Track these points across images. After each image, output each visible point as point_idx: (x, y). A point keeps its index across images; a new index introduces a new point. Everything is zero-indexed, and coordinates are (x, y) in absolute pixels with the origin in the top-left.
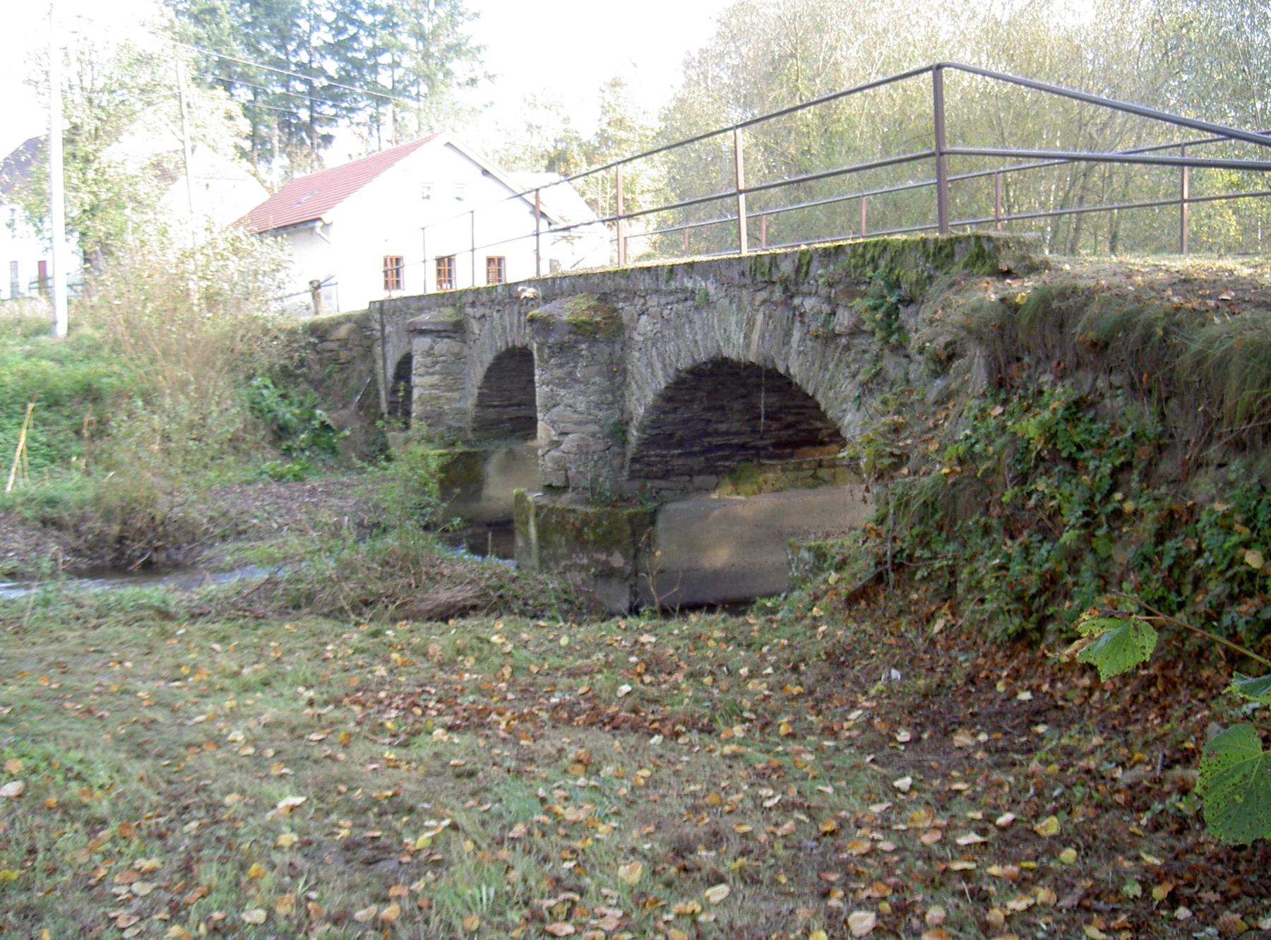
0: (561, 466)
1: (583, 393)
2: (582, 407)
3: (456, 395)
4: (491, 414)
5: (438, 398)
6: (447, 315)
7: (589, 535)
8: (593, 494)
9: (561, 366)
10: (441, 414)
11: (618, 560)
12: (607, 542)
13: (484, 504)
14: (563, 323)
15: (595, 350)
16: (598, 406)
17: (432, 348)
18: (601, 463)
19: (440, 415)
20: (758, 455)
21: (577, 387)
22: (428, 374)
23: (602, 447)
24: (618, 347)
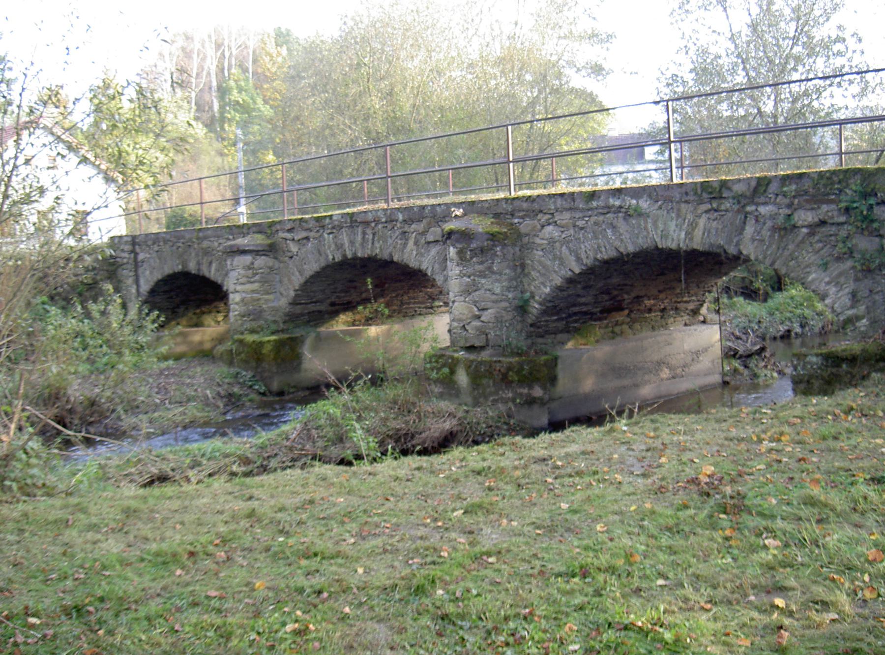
0: (482, 332)
1: (497, 281)
2: (498, 290)
3: (271, 297)
4: (298, 309)
5: (259, 300)
8: (504, 349)
9: (482, 263)
10: (261, 311)
11: (538, 392)
12: (529, 380)
13: (302, 374)
14: (481, 234)
15: (505, 251)
16: (508, 289)
17: (253, 263)
18: (511, 328)
19: (261, 312)
20: (591, 319)
23: (510, 317)
24: (517, 249)
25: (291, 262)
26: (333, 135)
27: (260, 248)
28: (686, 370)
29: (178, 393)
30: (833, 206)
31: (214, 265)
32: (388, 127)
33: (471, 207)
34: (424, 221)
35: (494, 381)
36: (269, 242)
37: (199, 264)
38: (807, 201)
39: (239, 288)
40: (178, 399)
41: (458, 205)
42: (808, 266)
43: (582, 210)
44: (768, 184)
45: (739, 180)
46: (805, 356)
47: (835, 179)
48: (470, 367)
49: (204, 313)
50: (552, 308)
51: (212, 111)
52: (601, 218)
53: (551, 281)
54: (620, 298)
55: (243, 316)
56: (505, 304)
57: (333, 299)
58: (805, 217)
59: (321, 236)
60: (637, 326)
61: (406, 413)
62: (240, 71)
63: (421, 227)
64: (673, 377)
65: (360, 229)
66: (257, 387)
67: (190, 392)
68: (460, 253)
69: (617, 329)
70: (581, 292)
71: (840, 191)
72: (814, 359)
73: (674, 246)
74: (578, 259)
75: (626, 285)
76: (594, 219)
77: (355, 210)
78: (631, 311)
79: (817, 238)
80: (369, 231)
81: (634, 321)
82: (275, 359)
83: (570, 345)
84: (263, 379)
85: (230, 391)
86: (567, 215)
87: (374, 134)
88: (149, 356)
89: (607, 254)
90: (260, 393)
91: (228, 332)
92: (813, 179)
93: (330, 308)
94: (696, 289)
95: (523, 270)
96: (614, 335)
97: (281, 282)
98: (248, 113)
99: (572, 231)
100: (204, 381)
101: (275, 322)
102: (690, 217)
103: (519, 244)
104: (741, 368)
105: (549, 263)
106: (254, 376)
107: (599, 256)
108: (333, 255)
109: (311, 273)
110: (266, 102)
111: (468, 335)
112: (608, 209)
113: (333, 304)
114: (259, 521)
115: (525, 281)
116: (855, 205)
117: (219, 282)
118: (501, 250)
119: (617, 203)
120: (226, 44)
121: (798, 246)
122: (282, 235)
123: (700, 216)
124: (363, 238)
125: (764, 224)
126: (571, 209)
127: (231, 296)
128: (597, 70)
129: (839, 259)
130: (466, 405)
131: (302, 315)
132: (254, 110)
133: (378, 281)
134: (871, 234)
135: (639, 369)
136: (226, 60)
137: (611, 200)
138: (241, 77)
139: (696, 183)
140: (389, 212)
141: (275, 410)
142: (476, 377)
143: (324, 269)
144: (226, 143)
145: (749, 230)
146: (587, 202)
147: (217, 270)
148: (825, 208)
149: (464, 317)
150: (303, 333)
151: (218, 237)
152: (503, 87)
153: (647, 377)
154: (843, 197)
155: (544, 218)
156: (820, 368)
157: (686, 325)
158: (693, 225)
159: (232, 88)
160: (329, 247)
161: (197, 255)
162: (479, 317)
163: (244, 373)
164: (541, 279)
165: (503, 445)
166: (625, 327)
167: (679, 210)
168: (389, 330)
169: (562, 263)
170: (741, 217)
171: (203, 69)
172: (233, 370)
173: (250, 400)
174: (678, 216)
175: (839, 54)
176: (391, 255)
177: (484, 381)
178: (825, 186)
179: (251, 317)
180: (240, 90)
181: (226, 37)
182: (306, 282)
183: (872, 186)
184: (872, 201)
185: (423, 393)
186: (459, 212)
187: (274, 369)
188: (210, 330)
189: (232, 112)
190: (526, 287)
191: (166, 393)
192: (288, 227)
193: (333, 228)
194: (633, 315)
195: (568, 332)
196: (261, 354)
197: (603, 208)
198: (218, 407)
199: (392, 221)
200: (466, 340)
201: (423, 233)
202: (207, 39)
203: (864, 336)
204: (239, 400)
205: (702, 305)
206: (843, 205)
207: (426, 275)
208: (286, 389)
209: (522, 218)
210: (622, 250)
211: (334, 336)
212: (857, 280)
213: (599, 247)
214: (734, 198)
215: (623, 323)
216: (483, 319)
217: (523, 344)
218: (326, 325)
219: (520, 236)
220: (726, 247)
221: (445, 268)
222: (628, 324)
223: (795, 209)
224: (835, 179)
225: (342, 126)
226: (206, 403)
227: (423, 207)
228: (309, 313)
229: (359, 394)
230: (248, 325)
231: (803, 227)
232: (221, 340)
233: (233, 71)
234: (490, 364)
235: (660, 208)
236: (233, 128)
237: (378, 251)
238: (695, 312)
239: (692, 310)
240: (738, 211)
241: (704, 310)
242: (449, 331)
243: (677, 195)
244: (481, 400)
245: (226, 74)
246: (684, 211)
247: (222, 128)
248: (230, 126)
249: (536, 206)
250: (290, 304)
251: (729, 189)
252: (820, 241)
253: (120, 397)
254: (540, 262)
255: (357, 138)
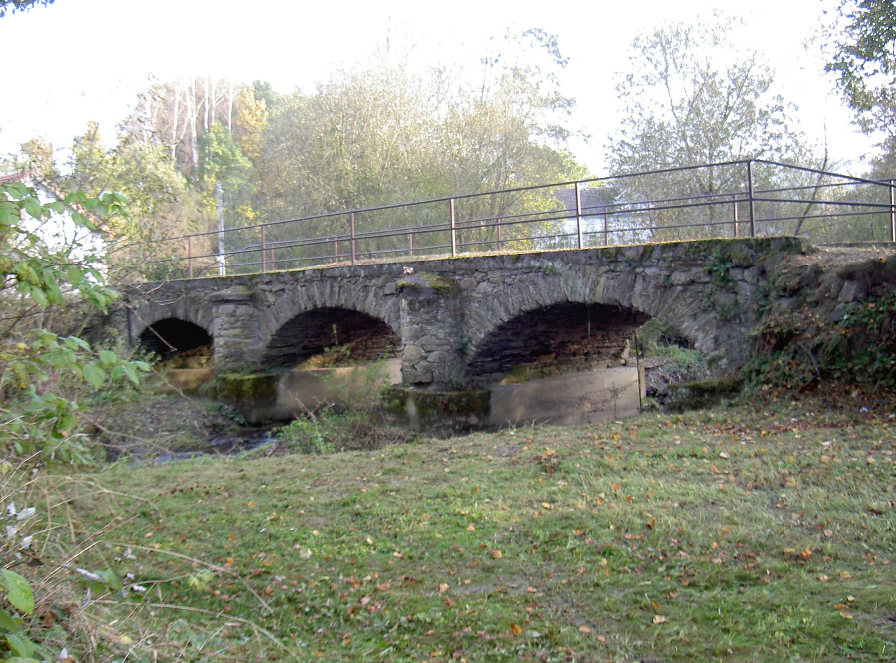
0: (428, 370)
1: (441, 327)
2: (441, 336)
4: (274, 352)
5: (240, 343)
6: (240, 291)
7: (453, 407)
8: (447, 385)
9: (428, 313)
14: (428, 288)
15: (448, 303)
16: (450, 335)
17: (235, 312)
21: (438, 324)
22: (232, 328)
23: (451, 358)
24: (458, 301)
25: (268, 311)
26: (309, 194)
27: (241, 298)
28: (606, 405)
29: (169, 423)
30: (701, 269)
31: (200, 313)
32: (359, 187)
33: (420, 266)
34: (383, 277)
35: (438, 412)
36: (249, 293)
37: (186, 311)
38: (681, 265)
39: (223, 333)
40: (169, 428)
41: (409, 264)
42: (682, 316)
43: (510, 270)
44: (652, 251)
45: (630, 248)
46: (677, 388)
47: (702, 248)
48: (417, 399)
49: (188, 356)
50: (487, 350)
51: (192, 162)
52: (525, 276)
53: (485, 328)
54: (546, 343)
55: (227, 357)
56: (446, 347)
57: (305, 343)
58: (680, 277)
59: (295, 288)
60: (564, 367)
61: (362, 435)
62: (220, 124)
63: (379, 282)
64: (595, 411)
65: (328, 283)
66: (237, 419)
67: (180, 422)
68: (411, 304)
69: (546, 370)
70: (511, 338)
71: (706, 257)
72: (684, 390)
73: (581, 300)
74: (507, 310)
75: (551, 332)
76: (519, 277)
77: (324, 266)
78: (557, 354)
79: (688, 294)
80: (336, 285)
81: (561, 363)
82: (254, 395)
83: (504, 382)
84: (243, 413)
85: (214, 422)
86: (497, 274)
87: (346, 193)
88: (147, 389)
89: (529, 306)
90: (240, 425)
91: (212, 371)
92: (685, 247)
93: (302, 351)
94: (615, 336)
95: (463, 319)
96: (542, 375)
97: (259, 328)
98: (227, 165)
99: (501, 287)
100: (193, 413)
101: (254, 363)
102: (593, 276)
103: (460, 297)
104: (657, 405)
105: (484, 313)
106: (235, 410)
107: (523, 308)
108: (305, 305)
109: (286, 320)
110: (244, 154)
111: (416, 373)
112: (530, 269)
113: (304, 348)
114: (249, 480)
115: (465, 328)
116: (715, 269)
117: (205, 327)
118: (445, 302)
119: (537, 265)
120: (206, 96)
121: (675, 300)
122: (261, 287)
123: (600, 276)
124: (331, 291)
125: (649, 283)
126: (501, 269)
127: (216, 340)
128: (560, 133)
129: (705, 311)
130: (414, 431)
131: (278, 357)
132: (233, 161)
133: (344, 328)
134: (728, 291)
135: (564, 403)
136: (206, 113)
137: (532, 262)
138: (221, 130)
139: (597, 249)
140: (353, 269)
141: (253, 438)
142: (423, 407)
143: (297, 317)
144: (205, 194)
145: (638, 287)
146: (514, 263)
147: (203, 317)
148: (694, 270)
149: (413, 358)
150: (279, 373)
151: (205, 288)
152: (465, 153)
153: (570, 410)
154: (707, 262)
155: (479, 276)
156: (688, 397)
157: (608, 367)
158: (596, 283)
159: (211, 140)
160: (302, 298)
161: (185, 303)
162: (425, 358)
163: (226, 407)
164: (477, 327)
165: (422, 443)
166: (552, 368)
167: (585, 271)
168: (354, 372)
169: (494, 313)
170: (632, 277)
171: (183, 121)
172: (217, 405)
173: (232, 430)
174: (584, 275)
175: (777, 122)
176: (354, 305)
177: (430, 411)
178: (694, 253)
179: (233, 358)
180: (220, 142)
181: (206, 90)
182: (282, 328)
183: (728, 253)
184: (728, 265)
185: (380, 422)
186: (410, 270)
187: (253, 403)
188: (195, 371)
189: (212, 163)
190: (465, 333)
191: (159, 423)
192: (267, 280)
193: (306, 281)
194: (559, 358)
195: (502, 371)
196: (241, 390)
197: (526, 268)
198: (204, 435)
199: (355, 277)
200: (415, 376)
201: (382, 287)
202: (187, 92)
203: (725, 371)
204: (222, 430)
205: (622, 350)
206: (707, 268)
207: (384, 322)
208: (263, 421)
209: (462, 275)
210: (541, 303)
211: (306, 376)
212: (718, 327)
213: (523, 300)
214: (626, 262)
215: (551, 365)
216: (429, 359)
217: (463, 380)
218: (299, 366)
219: (460, 290)
220: (621, 301)
221: (399, 318)
222: (555, 365)
223: (673, 271)
224: (702, 248)
225: (316, 186)
226: (193, 431)
227: (381, 265)
228: (284, 355)
229: (324, 419)
230: (230, 365)
231: (678, 285)
232: (204, 379)
233: (213, 123)
234: (434, 397)
235: (570, 269)
236: (213, 180)
237: (343, 302)
238: (617, 356)
239: (614, 355)
240: (630, 272)
241: (625, 354)
242: (402, 370)
243: (583, 259)
244: (427, 427)
245: (206, 126)
246: (588, 272)
247: (202, 178)
248: (209, 177)
249: (473, 266)
250: (268, 347)
251: (623, 254)
252: (690, 297)
253: (119, 426)
254: (477, 313)
255: (330, 197)
